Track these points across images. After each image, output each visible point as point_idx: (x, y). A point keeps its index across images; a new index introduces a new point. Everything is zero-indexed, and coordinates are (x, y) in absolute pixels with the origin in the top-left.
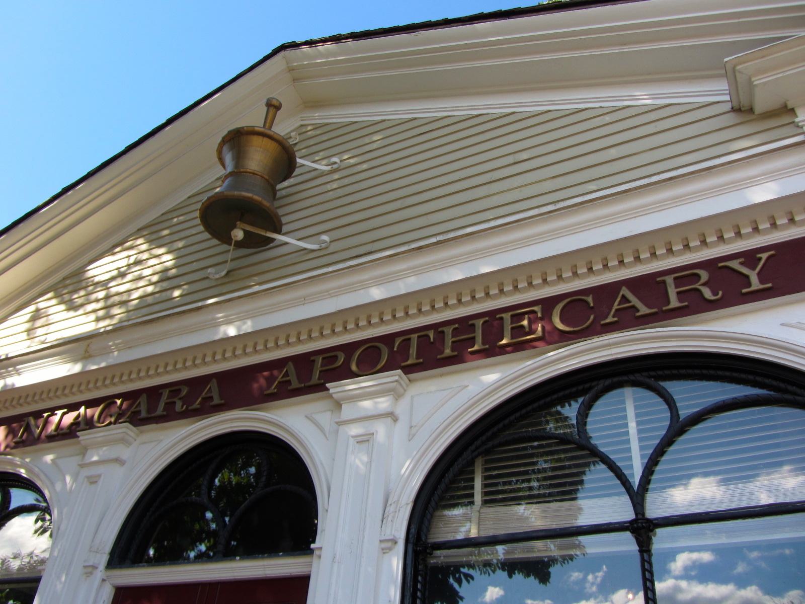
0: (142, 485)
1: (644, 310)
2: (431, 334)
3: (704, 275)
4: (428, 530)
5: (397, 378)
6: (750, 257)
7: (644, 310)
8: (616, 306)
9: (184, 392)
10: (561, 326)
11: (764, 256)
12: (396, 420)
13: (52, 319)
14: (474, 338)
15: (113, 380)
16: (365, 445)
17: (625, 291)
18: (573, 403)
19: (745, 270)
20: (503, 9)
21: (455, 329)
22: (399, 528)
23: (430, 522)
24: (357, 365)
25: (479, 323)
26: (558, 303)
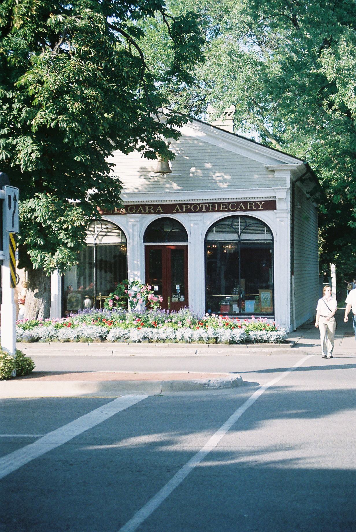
6: (261, 202)
11: (263, 203)
25: (216, 205)
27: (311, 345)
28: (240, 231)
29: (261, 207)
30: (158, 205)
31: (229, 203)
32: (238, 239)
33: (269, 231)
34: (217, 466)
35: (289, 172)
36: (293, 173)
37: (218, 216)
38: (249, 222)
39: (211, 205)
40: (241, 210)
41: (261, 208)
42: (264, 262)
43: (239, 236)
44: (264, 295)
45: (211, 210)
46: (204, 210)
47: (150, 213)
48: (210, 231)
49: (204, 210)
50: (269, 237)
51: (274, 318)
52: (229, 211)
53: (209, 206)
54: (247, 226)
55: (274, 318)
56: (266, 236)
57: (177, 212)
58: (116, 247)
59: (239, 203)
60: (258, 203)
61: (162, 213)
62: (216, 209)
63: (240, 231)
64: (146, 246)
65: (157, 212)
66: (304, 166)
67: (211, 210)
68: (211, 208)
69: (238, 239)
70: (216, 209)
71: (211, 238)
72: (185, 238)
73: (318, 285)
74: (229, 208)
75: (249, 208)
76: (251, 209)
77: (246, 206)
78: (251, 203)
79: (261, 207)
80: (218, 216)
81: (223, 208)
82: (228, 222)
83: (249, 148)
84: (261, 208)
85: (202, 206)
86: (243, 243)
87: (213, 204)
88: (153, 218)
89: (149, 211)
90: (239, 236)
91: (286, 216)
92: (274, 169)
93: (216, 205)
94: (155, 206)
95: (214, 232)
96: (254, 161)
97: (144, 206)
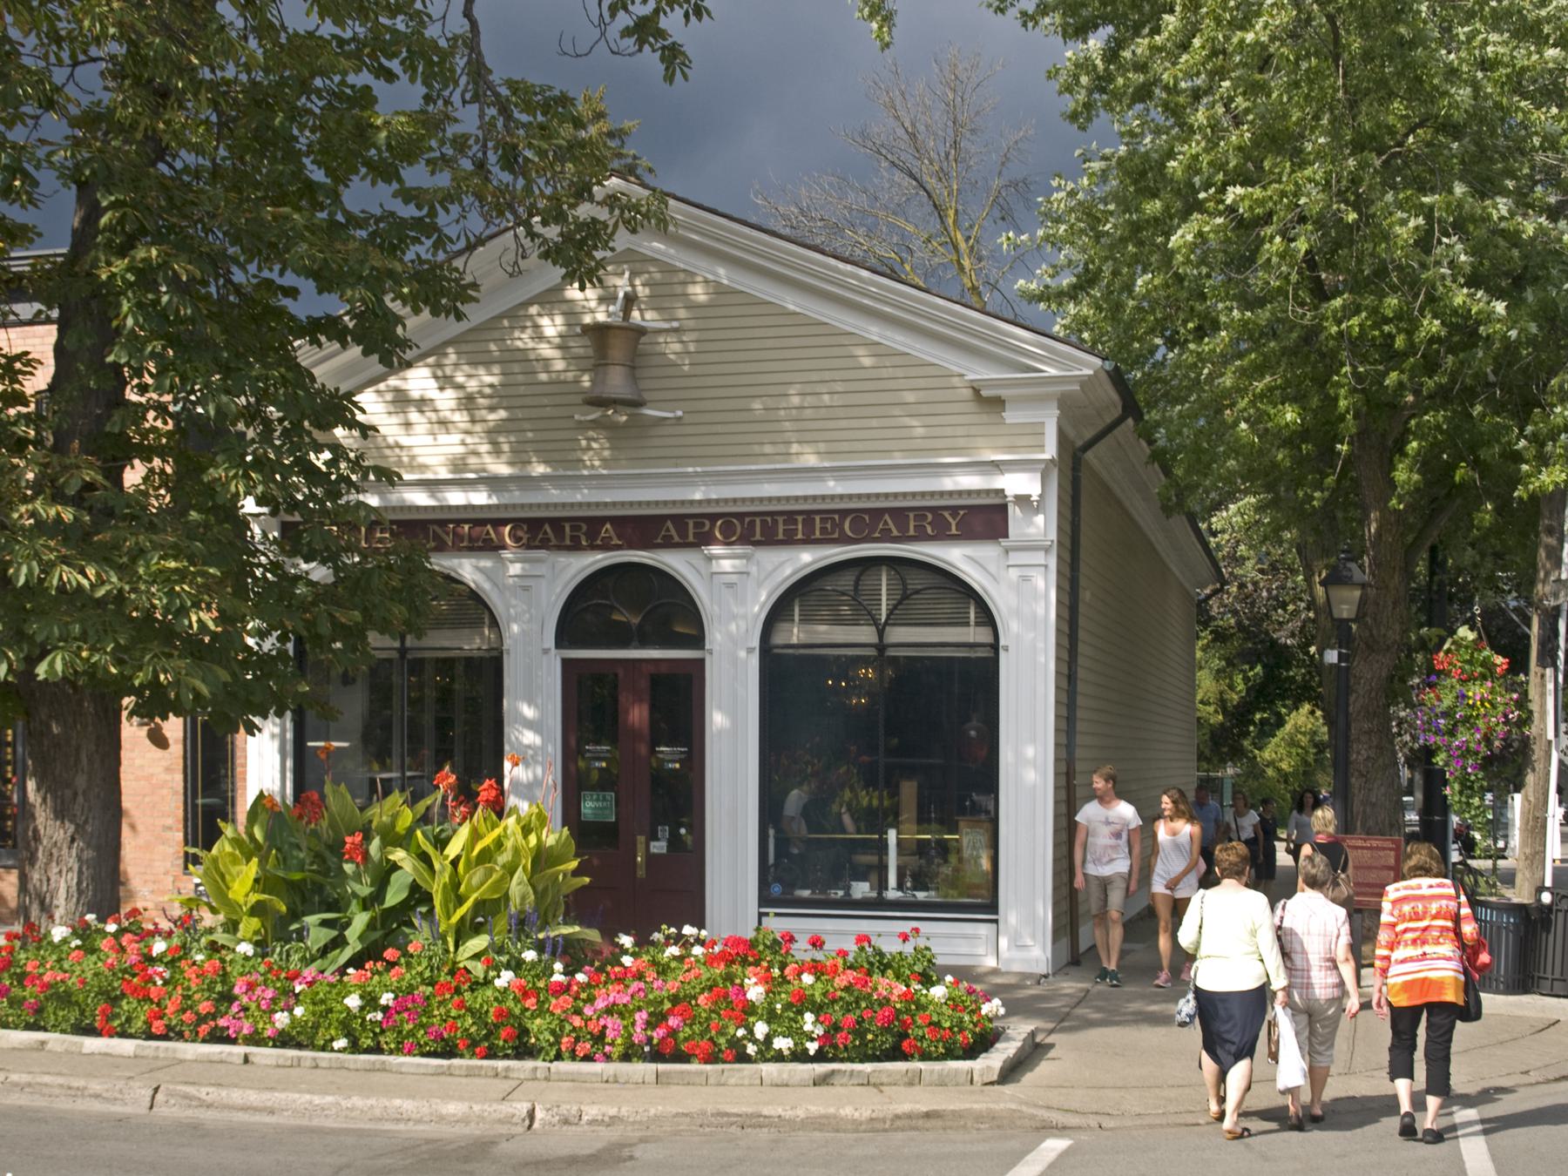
3: (930, 517)
7: (895, 533)
25: (800, 518)
27: (1022, 1102)
28: (884, 607)
30: (603, 520)
31: (844, 513)
33: (987, 618)
35: (1055, 404)
36: (1067, 406)
37: (807, 558)
38: (916, 581)
39: (780, 519)
40: (886, 537)
41: (954, 531)
42: (974, 723)
43: (881, 633)
44: (968, 838)
45: (781, 537)
46: (758, 537)
47: (575, 547)
48: (778, 612)
49: (758, 537)
50: (980, 635)
51: (996, 921)
52: (844, 540)
53: (775, 522)
54: (905, 597)
55: (996, 921)
56: (975, 634)
57: (668, 544)
59: (877, 513)
60: (946, 514)
61: (618, 548)
62: (800, 536)
63: (884, 607)
64: (567, 664)
67: (781, 537)
68: (781, 528)
70: (800, 536)
71: (794, 633)
74: (842, 531)
75: (912, 532)
76: (921, 537)
77: (903, 527)
78: (920, 512)
80: (807, 558)
81: (823, 530)
82: (846, 581)
84: (954, 531)
85: (752, 523)
87: (790, 516)
89: (573, 538)
90: (881, 633)
92: (1003, 393)
93: (800, 518)
94: (595, 523)
95: (797, 618)
96: (795, 313)
97: (557, 523)
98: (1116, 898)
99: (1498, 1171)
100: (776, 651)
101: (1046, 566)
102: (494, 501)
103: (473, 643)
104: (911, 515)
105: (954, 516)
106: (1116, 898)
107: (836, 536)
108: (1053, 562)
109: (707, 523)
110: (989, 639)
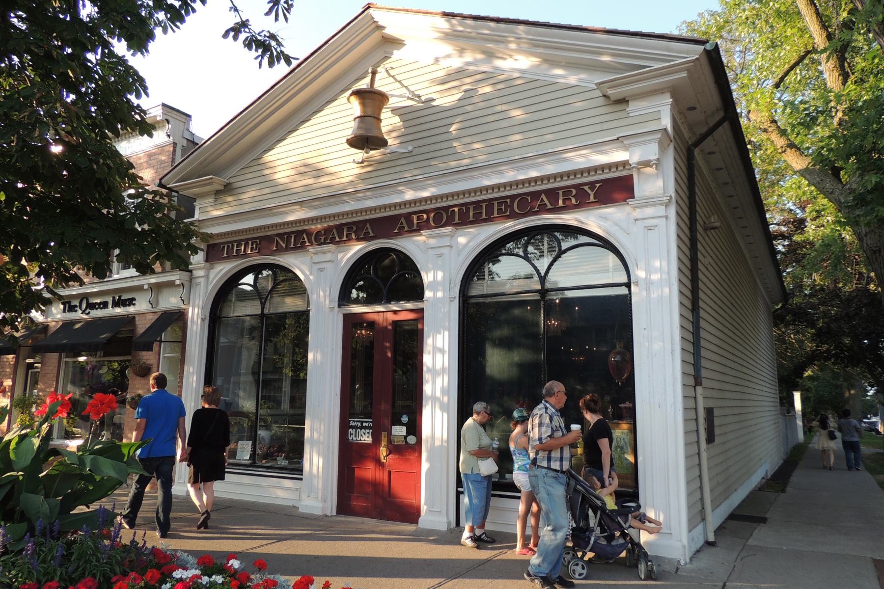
0: (241, 484)
1: (549, 206)
2: (464, 208)
3: (574, 192)
4: (468, 291)
5: (450, 230)
6: (592, 184)
7: (549, 206)
8: (539, 203)
9: (355, 228)
10: (517, 211)
11: (598, 185)
12: (452, 247)
13: (143, 154)
14: (482, 212)
15: (222, 190)
16: (440, 258)
17: (543, 196)
18: (826, 199)
19: (589, 191)
20: (511, 18)
21: (474, 207)
22: (456, 293)
23: (468, 288)
24: (434, 222)
25: (484, 205)
26: (444, 224)
29: (592, 197)
30: (364, 222)
32: (540, 288)
34: (630, 580)
41: (592, 199)
46: (457, 221)
49: (457, 221)
52: (514, 216)
58: (625, 296)
60: (586, 188)
62: (484, 216)
65: (362, 236)
66: (705, 62)
69: (539, 287)
72: (416, 291)
73: (780, 416)
74: (512, 210)
79: (592, 197)
81: (499, 211)
83: (754, 327)
84: (592, 199)
86: (478, 304)
88: (356, 249)
91: (664, 214)
98: (817, 419)
99: (881, 587)
100: (473, 301)
101: (667, 217)
102: (383, 264)
103: (291, 304)
104: (561, 192)
105: (592, 189)
106: (817, 419)
107: (508, 213)
108: (672, 212)
109: (425, 216)
110: (625, 280)
